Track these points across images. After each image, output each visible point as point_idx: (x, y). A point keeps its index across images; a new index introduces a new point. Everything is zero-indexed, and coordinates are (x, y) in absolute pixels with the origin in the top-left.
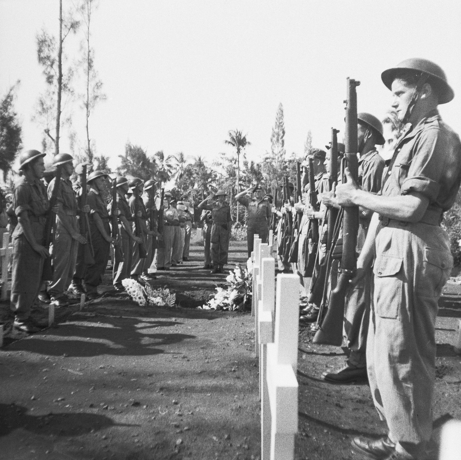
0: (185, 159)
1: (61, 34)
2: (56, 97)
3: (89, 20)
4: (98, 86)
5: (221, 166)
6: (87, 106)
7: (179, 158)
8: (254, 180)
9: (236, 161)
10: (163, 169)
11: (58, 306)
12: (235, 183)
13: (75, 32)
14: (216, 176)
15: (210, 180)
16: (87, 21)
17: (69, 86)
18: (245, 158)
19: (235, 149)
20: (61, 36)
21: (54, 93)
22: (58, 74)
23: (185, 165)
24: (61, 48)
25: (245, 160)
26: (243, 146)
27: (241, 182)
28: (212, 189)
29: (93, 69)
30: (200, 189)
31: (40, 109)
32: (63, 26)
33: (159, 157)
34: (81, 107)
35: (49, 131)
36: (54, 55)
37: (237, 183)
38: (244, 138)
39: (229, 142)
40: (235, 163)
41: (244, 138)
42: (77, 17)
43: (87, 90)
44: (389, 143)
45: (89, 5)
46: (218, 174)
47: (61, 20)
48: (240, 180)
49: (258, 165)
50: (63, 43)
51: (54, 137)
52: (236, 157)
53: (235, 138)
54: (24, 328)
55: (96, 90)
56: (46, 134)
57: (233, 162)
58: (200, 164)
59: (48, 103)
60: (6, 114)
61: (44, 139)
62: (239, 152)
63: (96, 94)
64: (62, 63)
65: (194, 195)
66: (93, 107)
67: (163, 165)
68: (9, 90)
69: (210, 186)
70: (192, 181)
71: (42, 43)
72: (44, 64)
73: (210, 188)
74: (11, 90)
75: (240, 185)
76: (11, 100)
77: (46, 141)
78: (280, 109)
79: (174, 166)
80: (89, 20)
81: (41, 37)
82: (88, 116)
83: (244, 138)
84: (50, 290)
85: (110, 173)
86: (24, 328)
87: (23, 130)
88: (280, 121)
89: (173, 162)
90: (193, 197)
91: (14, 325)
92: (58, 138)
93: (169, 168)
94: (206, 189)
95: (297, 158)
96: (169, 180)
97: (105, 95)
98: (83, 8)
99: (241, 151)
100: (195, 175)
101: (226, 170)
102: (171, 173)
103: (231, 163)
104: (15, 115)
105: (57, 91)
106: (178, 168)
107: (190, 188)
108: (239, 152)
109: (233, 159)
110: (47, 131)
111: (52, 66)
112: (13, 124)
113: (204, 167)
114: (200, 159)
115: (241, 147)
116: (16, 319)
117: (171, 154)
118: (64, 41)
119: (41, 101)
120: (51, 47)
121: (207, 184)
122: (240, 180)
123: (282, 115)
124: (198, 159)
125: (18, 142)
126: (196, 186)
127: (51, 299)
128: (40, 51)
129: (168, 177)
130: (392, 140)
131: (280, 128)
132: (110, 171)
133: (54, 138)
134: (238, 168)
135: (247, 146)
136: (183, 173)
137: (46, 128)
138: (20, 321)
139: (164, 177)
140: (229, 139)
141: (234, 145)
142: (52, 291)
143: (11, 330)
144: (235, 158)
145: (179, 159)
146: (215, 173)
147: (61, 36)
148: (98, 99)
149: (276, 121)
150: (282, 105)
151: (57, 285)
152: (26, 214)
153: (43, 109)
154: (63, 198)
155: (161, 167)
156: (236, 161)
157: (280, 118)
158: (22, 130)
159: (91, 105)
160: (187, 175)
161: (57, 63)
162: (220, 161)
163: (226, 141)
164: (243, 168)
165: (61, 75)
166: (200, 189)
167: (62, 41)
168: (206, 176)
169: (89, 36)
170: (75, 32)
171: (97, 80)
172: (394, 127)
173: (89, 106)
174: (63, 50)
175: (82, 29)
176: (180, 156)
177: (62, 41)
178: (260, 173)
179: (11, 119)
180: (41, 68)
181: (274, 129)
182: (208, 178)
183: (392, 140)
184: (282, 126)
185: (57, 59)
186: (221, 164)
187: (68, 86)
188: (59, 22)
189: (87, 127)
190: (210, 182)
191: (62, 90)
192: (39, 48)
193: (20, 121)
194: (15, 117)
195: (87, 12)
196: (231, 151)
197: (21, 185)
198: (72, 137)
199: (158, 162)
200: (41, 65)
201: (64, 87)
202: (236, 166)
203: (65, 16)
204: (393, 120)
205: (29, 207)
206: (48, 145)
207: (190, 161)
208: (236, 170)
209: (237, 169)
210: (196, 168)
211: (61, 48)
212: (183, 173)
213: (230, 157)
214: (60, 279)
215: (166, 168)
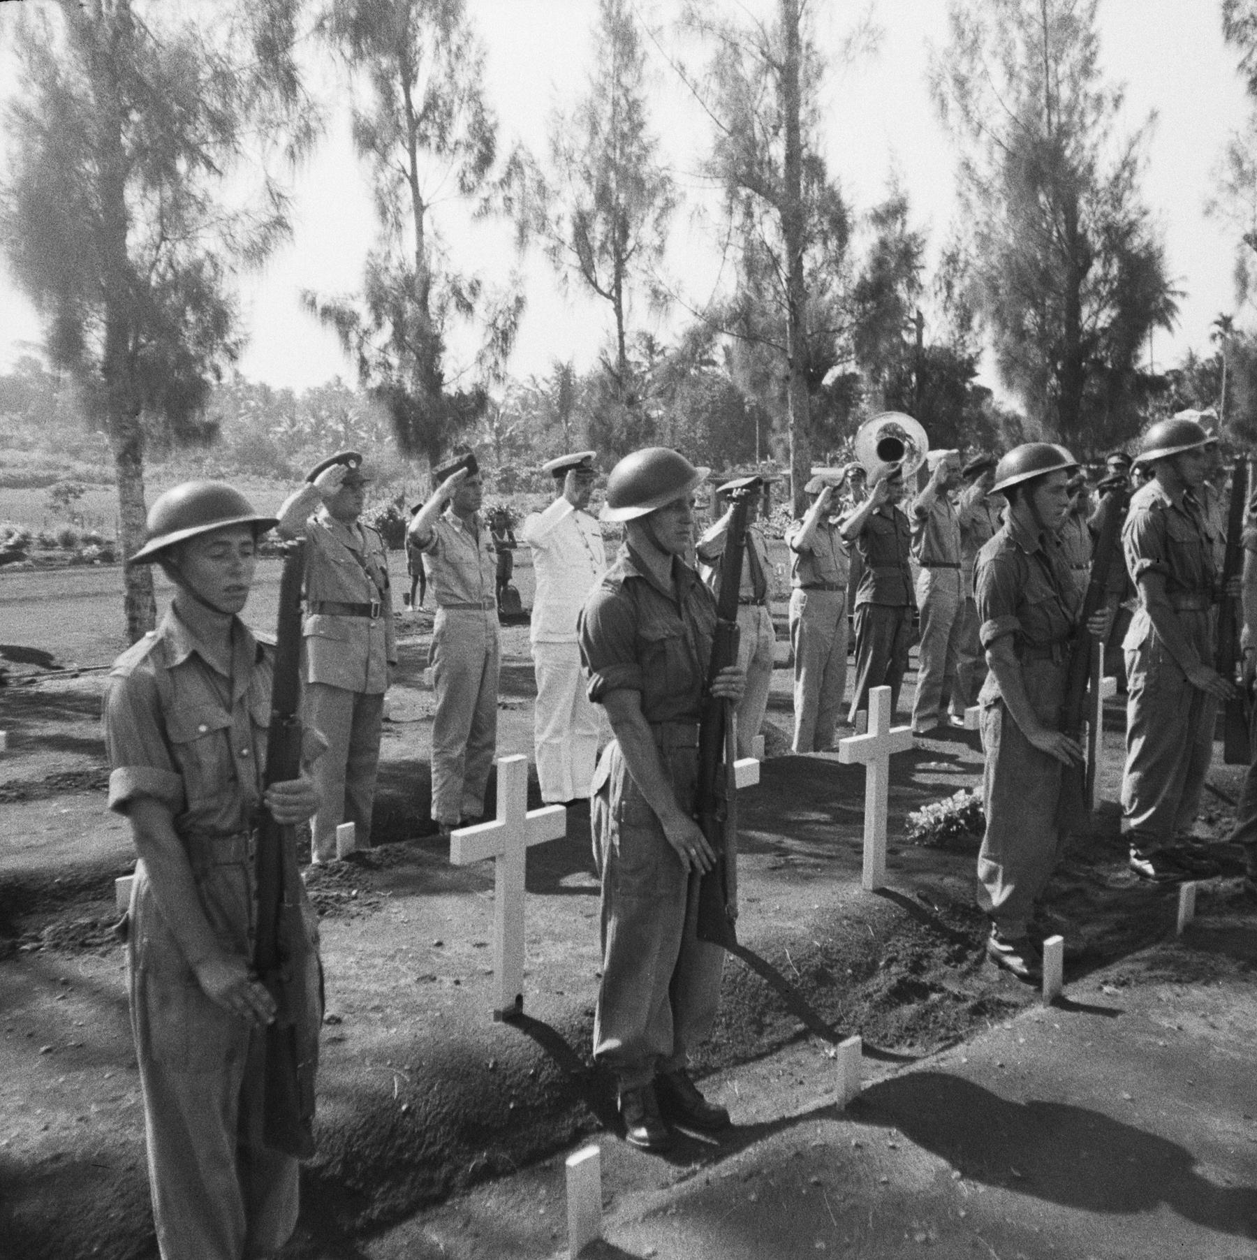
31: (1230, 175)
60: (1119, 216)
68: (1124, 148)
72: (1241, 42)
74: (1132, 144)
76: (1132, 174)
86: (1016, 962)
91: (990, 948)
104: (1145, 213)
112: (1136, 243)
116: (994, 932)
119: (1233, 152)
138: (1002, 941)
143: (981, 960)
152: (1008, 642)
153: (1243, 175)
154: (1168, 560)
158: (1166, 255)
179: (1132, 227)
193: (1158, 228)
194: (1146, 219)
197: (994, 560)
200: (1234, 44)
205: (1015, 624)
214: (685, 1131)
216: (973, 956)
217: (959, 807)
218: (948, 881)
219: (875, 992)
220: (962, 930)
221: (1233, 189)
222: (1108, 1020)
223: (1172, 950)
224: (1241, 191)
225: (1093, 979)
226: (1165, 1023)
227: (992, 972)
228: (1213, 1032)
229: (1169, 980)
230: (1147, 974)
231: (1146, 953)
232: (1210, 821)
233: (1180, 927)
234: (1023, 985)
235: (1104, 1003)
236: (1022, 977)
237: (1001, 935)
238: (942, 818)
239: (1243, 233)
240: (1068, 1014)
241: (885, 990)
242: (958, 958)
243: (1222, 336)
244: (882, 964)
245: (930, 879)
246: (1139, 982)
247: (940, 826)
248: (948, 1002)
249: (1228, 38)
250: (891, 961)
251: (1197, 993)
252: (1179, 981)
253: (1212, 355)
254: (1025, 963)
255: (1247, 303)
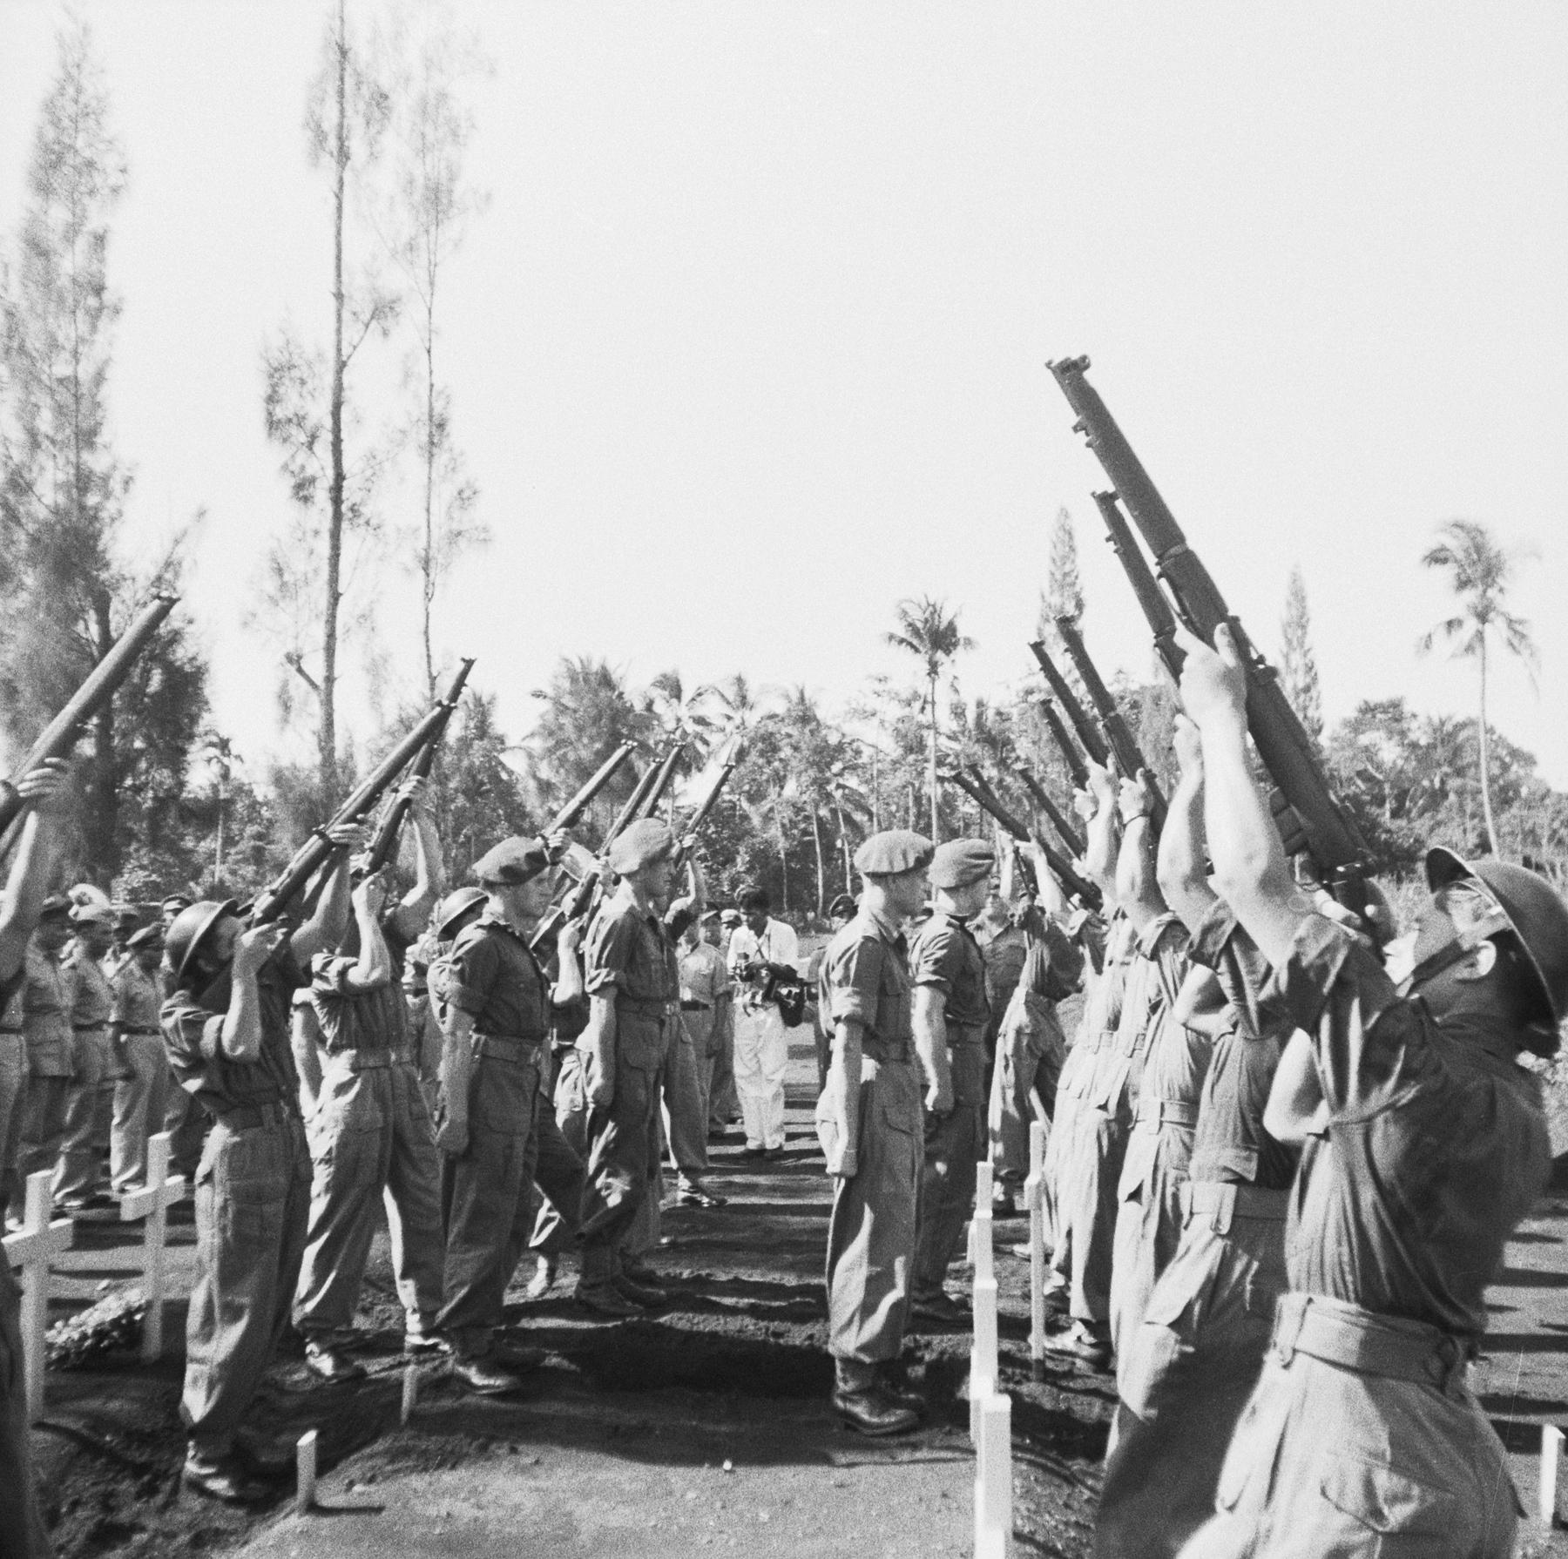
0: (751, 697)
1: (339, 342)
2: (324, 546)
3: (432, 284)
4: (464, 497)
5: (875, 721)
6: (426, 564)
7: (731, 694)
8: (987, 763)
9: (927, 703)
10: (678, 733)
11: (329, 1378)
12: (921, 774)
13: (385, 333)
14: (858, 753)
15: (837, 767)
16: (426, 288)
17: (366, 511)
18: (956, 691)
19: (920, 663)
20: (339, 350)
21: (317, 533)
22: (330, 473)
23: (752, 718)
24: (339, 388)
25: (954, 698)
26: (948, 652)
27: (945, 772)
28: (844, 795)
29: (446, 445)
30: (805, 798)
31: (271, 585)
32: (346, 315)
33: (666, 693)
34: (407, 570)
35: (300, 657)
36: (319, 413)
37: (931, 772)
38: (951, 628)
39: (902, 641)
40: (923, 709)
41: (951, 624)
42: (395, 280)
43: (424, 513)
44: (1449, 632)
45: (432, 238)
46: (863, 748)
47: (339, 296)
48: (940, 763)
49: (999, 713)
50: (346, 370)
51: (318, 675)
52: (924, 687)
53: (920, 625)
54: (220, 1485)
55: (456, 514)
56: (293, 669)
57: (917, 705)
58: (806, 718)
59: (298, 565)
61: (285, 685)
62: (933, 668)
63: (455, 527)
64: (343, 435)
65: (786, 821)
66: (446, 567)
67: (679, 720)
68: (168, 545)
69: (839, 786)
70: (776, 772)
71: (278, 373)
72: (285, 440)
73: (838, 794)
74: (177, 542)
75: (941, 779)
76: (177, 575)
77: (293, 691)
78: (1063, 527)
79: (718, 721)
80: (432, 284)
81: (277, 354)
82: (428, 597)
83: (951, 624)
84: (302, 1321)
85: (503, 750)
86: (220, 1485)
87: (213, 668)
88: (1067, 568)
89: (712, 709)
90: (783, 825)
92: (330, 680)
93: (699, 729)
94: (829, 797)
95: (1134, 687)
96: (700, 770)
97: (485, 530)
98: (411, 248)
99: (940, 669)
100: (786, 752)
101: (890, 731)
102: (706, 743)
103: (908, 709)
104: (191, 622)
105: (326, 524)
106: (730, 727)
107: (773, 791)
108: (933, 668)
109: (916, 696)
110: (294, 660)
111: (310, 445)
112: (180, 654)
113: (819, 724)
114: (802, 699)
115: (940, 655)
117: (705, 682)
118: (350, 363)
119: (274, 560)
120: (310, 386)
121: (828, 782)
122: (940, 763)
123: (1072, 549)
124: (795, 697)
125: (200, 709)
126: (791, 789)
127: (308, 1350)
128: (272, 399)
129: (698, 757)
130: (1460, 623)
131: (1068, 592)
132: (502, 742)
133: (319, 679)
134: (932, 726)
135: (959, 653)
136: (746, 743)
137: (290, 647)
138: (203, 1462)
139: (686, 762)
140: (902, 632)
141: (917, 650)
142: (308, 1325)
143: (175, 1491)
144: (922, 692)
145: (731, 699)
146: (855, 745)
147: (339, 350)
148: (462, 542)
149: (1053, 569)
150: (1067, 516)
151: (326, 1295)
153: (283, 585)
155: (670, 726)
156: (927, 703)
157: (1064, 559)
159: (440, 559)
160: (762, 754)
161: (326, 437)
162: (872, 703)
163: (891, 637)
164: (947, 723)
165: (340, 477)
166: (805, 798)
167: (341, 366)
168: (825, 755)
169: (433, 337)
170: (385, 333)
171: (460, 480)
172: (1463, 577)
173: (432, 564)
174: (346, 394)
175: (407, 330)
176: (735, 688)
177: (341, 366)
178: (1007, 742)
180: (276, 454)
181: (1047, 594)
182: (833, 760)
183: (1460, 623)
184: (1073, 584)
185: (328, 422)
186: (873, 715)
187: (362, 509)
188: (332, 303)
189: (426, 633)
190: (840, 774)
191: (345, 525)
192: (269, 391)
194: (189, 629)
195: (424, 256)
196: (909, 667)
198: (376, 669)
199: (659, 707)
200: (277, 443)
201: (350, 515)
202: (925, 719)
203: (355, 284)
204: (1460, 555)
206: (295, 705)
207: (770, 703)
208: (925, 733)
209: (928, 727)
210: (789, 730)
211: (339, 388)
212: (746, 743)
213: (904, 688)
214: (332, 1276)
215: (691, 728)
216: (167, 1486)
217: (109, 1317)
218: (114, 1405)
219: (70, 1541)
220: (144, 1459)
221: (274, 601)
222: (375, 1519)
223: (405, 1439)
224: (282, 604)
225: (353, 1468)
226: (432, 1511)
227: (194, 1503)
228: (480, 1514)
229: (412, 1470)
230: (389, 1468)
231: (379, 1446)
232: (366, 1311)
233: (404, 1417)
234: (230, 1511)
235: (362, 1502)
236: (229, 1502)
237: (200, 1455)
238: (90, 1331)
239: (285, 651)
240: (326, 1521)
241: (81, 1537)
242: (150, 1491)
243: (219, 761)
244: (64, 1510)
245: (94, 1404)
246: (386, 1478)
247: (88, 1343)
248: (159, 1540)
249: (270, 435)
250: (75, 1505)
251: (448, 1478)
252: (425, 1470)
253: (206, 783)
254: (232, 1485)
255: (289, 728)
